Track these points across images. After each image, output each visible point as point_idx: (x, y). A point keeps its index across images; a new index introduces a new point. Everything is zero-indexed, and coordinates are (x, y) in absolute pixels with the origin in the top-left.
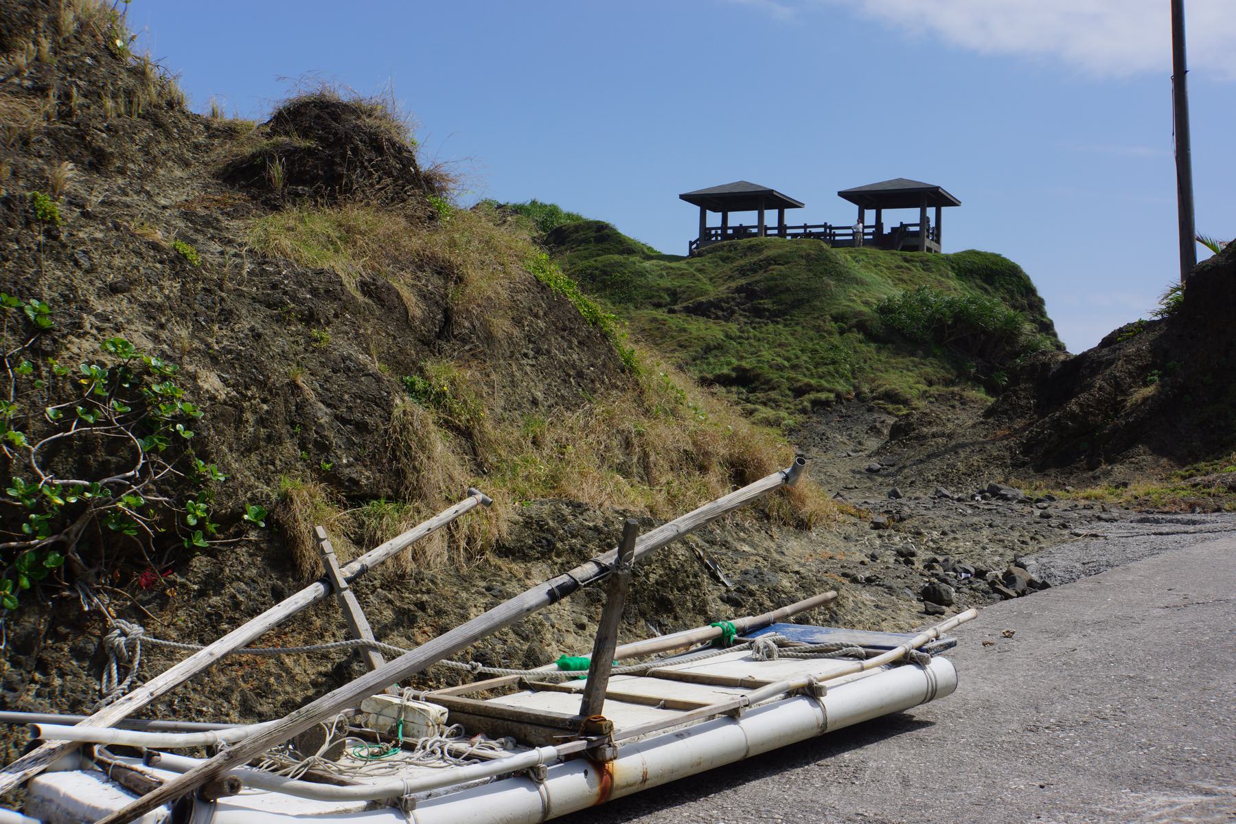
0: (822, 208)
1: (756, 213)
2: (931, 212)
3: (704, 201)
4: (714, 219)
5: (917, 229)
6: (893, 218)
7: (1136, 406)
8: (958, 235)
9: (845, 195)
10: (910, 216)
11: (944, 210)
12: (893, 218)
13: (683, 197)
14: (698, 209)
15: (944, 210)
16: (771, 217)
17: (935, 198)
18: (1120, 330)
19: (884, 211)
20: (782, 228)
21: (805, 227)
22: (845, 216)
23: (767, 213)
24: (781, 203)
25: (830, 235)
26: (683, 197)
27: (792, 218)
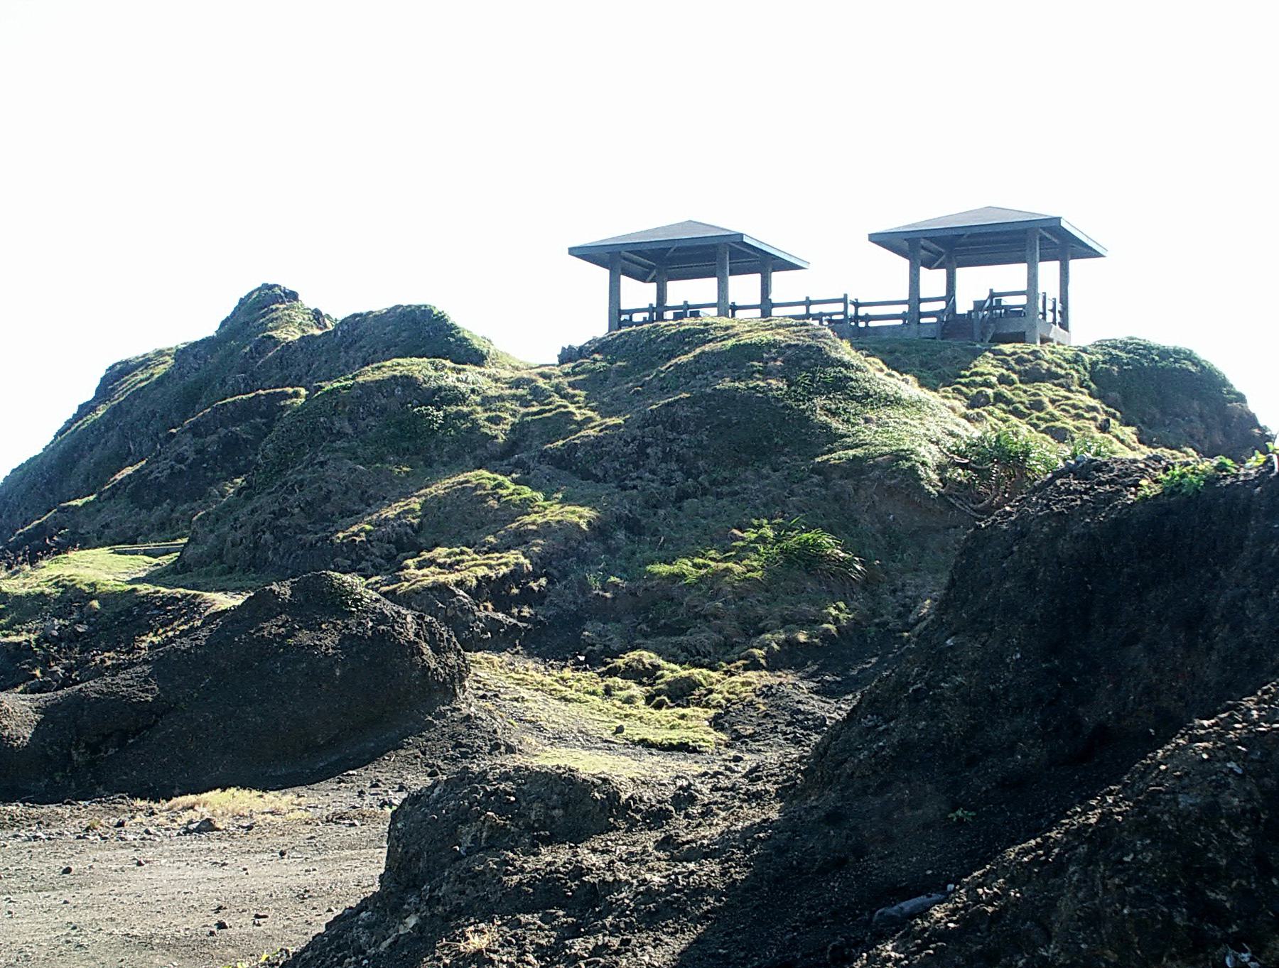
0: (842, 270)
1: (713, 282)
2: (1049, 271)
3: (621, 259)
4: (638, 294)
5: (1022, 300)
6: (976, 284)
7: (238, 590)
8: (1102, 310)
9: (884, 240)
10: (1005, 279)
11: (1074, 264)
12: (976, 284)
13: (574, 252)
14: (605, 273)
15: (1074, 264)
16: (744, 288)
17: (1047, 241)
18: (104, 379)
19: (960, 272)
20: (766, 306)
21: (808, 303)
22: (883, 283)
23: (735, 282)
24: (763, 262)
25: (857, 318)
26: (574, 252)
27: (784, 286)
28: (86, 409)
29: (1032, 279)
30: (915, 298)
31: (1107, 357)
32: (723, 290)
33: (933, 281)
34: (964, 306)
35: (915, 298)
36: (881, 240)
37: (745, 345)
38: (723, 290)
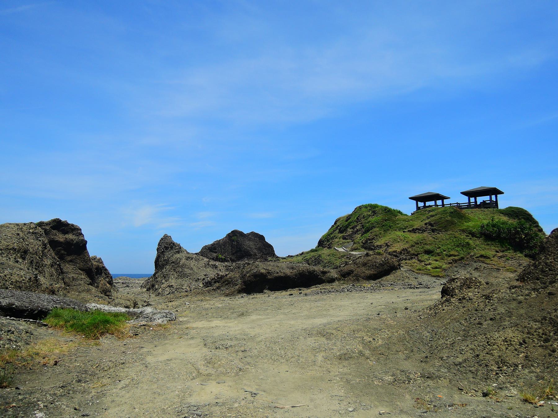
2: (493, 197)
3: (417, 199)
4: (421, 204)
8: (503, 203)
13: (410, 198)
16: (439, 202)
17: (496, 192)
20: (443, 205)
21: (451, 204)
22: (464, 200)
24: (443, 198)
26: (410, 198)
27: (446, 202)
28: (333, 226)
29: (491, 198)
30: (469, 202)
31: (532, 244)
32: (436, 203)
33: (472, 200)
34: (478, 203)
35: (469, 202)
36: (462, 193)
37: (276, 277)
38: (436, 203)
